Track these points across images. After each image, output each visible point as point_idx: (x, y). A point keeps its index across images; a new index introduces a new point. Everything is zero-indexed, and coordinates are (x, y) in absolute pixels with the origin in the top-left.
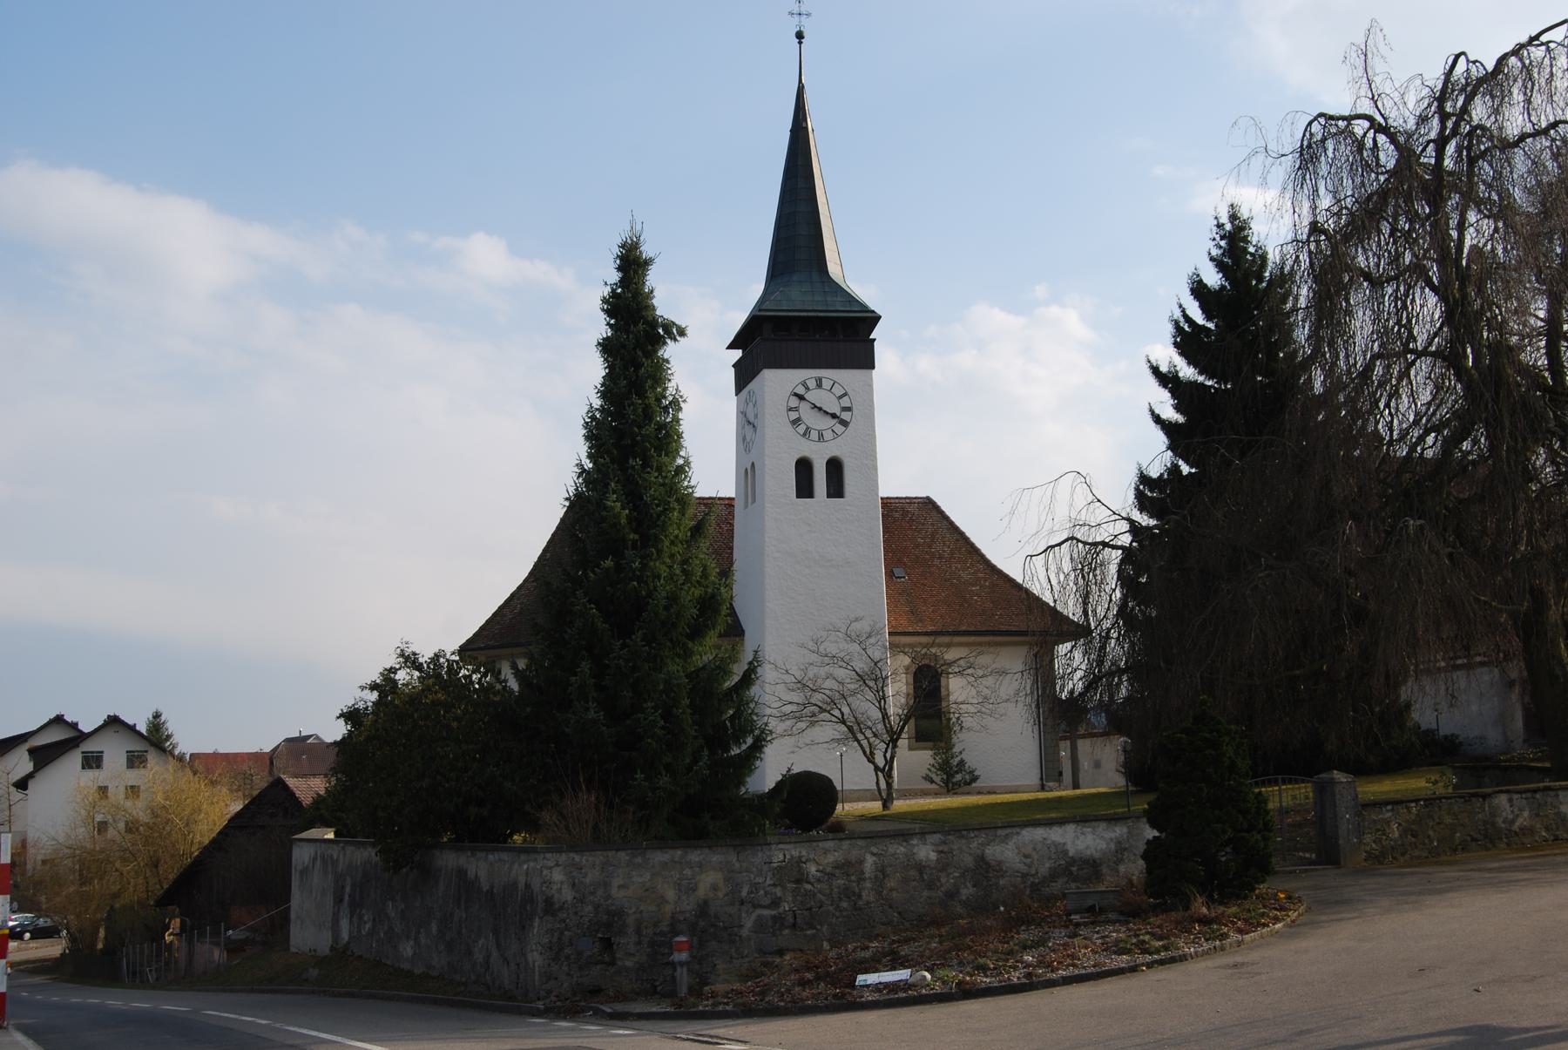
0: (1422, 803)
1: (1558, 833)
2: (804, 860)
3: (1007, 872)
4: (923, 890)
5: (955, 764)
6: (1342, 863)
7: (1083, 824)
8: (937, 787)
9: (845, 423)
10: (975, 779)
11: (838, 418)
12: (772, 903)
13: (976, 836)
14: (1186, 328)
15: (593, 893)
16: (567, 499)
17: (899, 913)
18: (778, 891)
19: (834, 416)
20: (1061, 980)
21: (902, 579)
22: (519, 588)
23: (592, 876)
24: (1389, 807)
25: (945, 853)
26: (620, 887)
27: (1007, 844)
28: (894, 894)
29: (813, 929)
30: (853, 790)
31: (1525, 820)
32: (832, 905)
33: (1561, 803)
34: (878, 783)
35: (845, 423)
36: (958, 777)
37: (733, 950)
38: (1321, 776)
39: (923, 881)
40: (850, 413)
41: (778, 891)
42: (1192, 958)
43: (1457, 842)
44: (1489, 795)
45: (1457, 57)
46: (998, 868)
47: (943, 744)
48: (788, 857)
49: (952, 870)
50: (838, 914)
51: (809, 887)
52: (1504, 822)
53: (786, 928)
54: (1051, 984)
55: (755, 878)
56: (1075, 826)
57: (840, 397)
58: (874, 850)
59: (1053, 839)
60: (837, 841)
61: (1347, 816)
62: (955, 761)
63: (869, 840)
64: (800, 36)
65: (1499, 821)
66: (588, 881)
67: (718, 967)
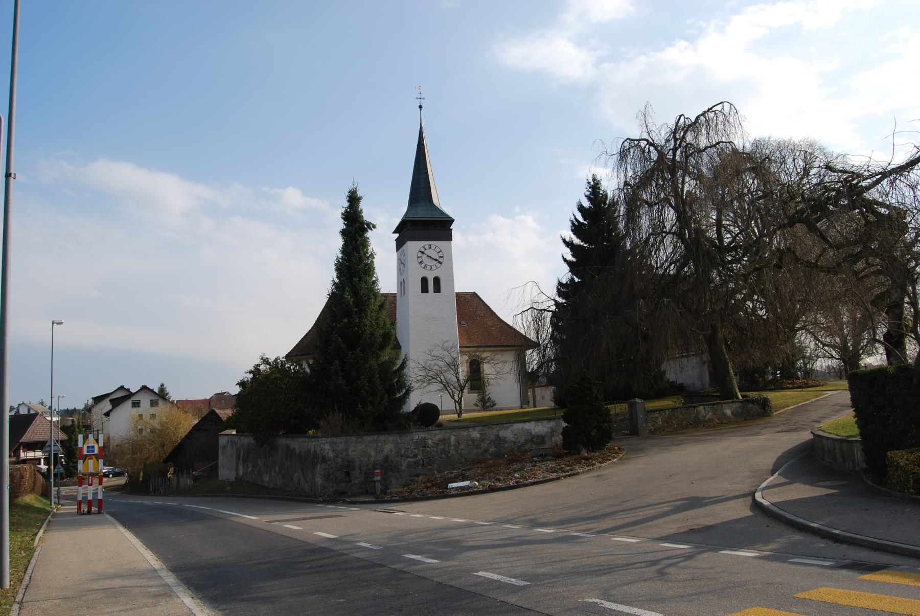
9: (440, 263)
10: (495, 405)
14: (576, 223)
15: (342, 454)
16: (328, 295)
17: (465, 459)
19: (436, 260)
23: (341, 446)
24: (658, 412)
26: (352, 451)
28: (463, 451)
34: (456, 407)
35: (440, 263)
36: (488, 404)
40: (442, 259)
41: (416, 451)
43: (684, 425)
45: (680, 116)
48: (420, 437)
51: (428, 449)
53: (420, 466)
54: (526, 485)
58: (454, 434)
64: (420, 107)
65: (700, 416)
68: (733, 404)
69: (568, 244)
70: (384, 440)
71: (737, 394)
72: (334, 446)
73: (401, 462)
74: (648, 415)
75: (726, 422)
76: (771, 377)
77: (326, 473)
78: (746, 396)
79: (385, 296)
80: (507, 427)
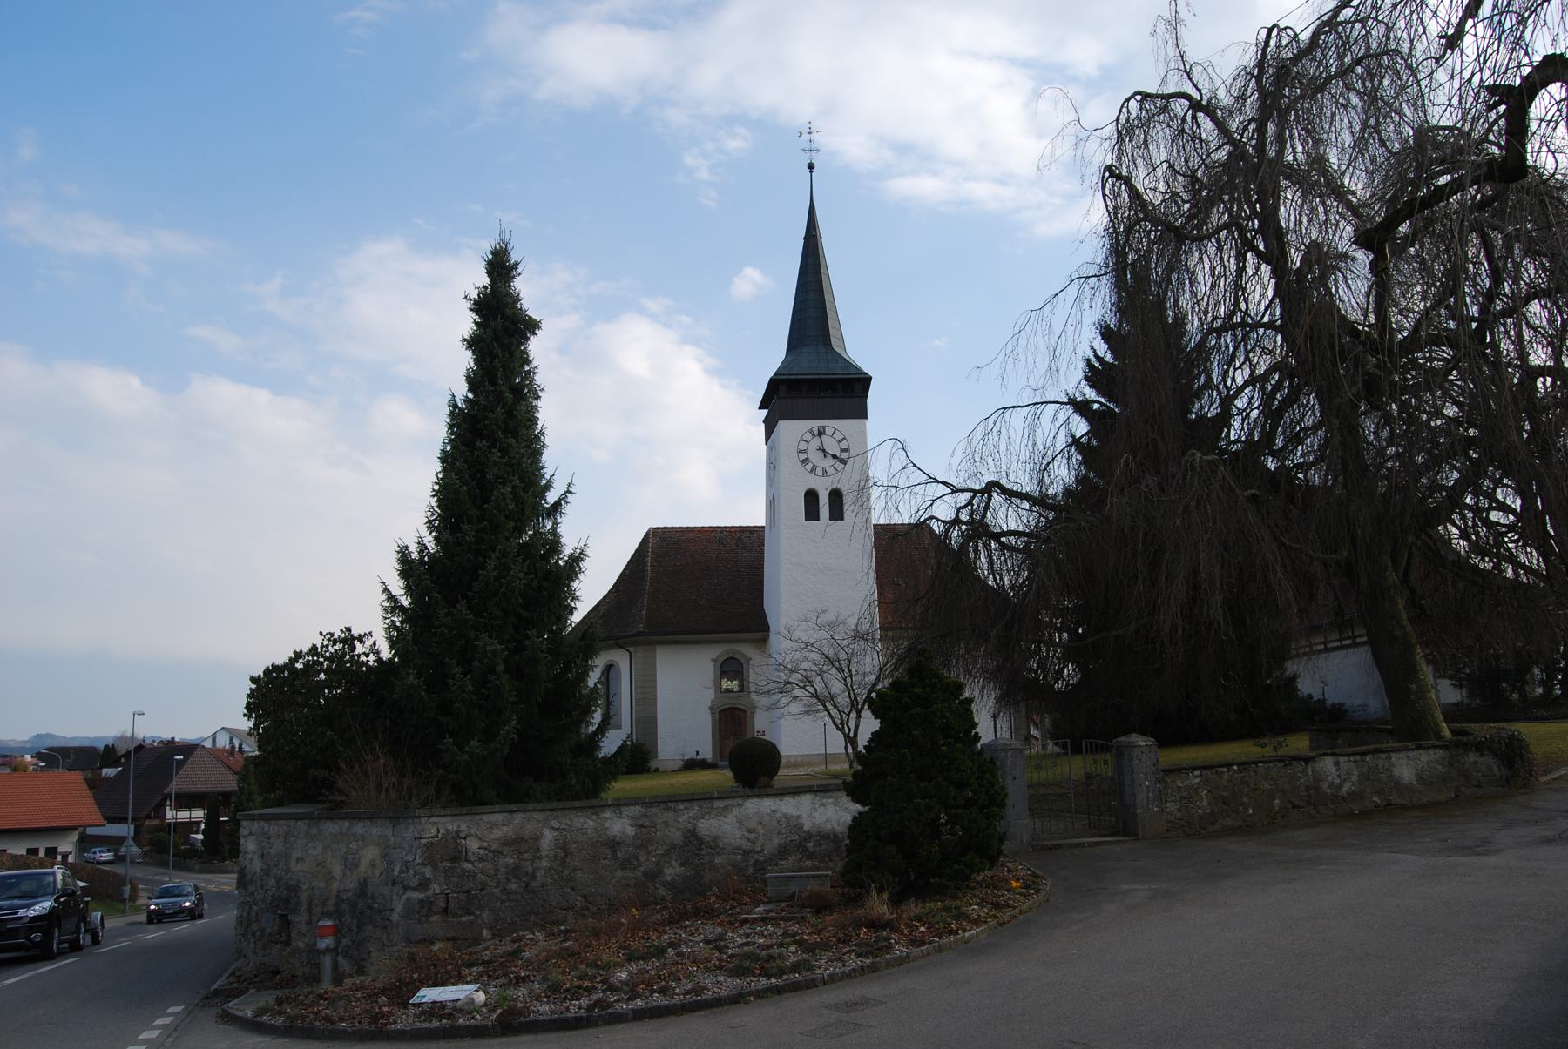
0: (1235, 767)
1: (1390, 797)
2: (462, 835)
3: (724, 849)
4: (617, 869)
6: (1140, 835)
7: (822, 794)
9: (844, 462)
12: (419, 885)
13: (686, 808)
14: (1097, 365)
15: (276, 865)
16: (436, 483)
17: (584, 896)
18: (428, 871)
20: (630, 1013)
23: (277, 847)
24: (1197, 773)
25: (645, 827)
26: (298, 860)
27: (726, 817)
28: (579, 874)
29: (470, 914)
31: (1354, 785)
32: (497, 887)
33: (1393, 766)
34: (846, 748)
35: (844, 462)
37: (385, 936)
38: (1119, 739)
39: (617, 859)
41: (428, 871)
42: (825, 984)
44: (1312, 759)
45: (1270, 30)
46: (713, 844)
48: (442, 832)
49: (654, 848)
50: (503, 897)
51: (468, 866)
52: (1330, 787)
53: (436, 914)
54: (619, 1019)
55: (406, 856)
56: (813, 796)
57: (840, 441)
58: (555, 824)
59: (784, 811)
60: (505, 814)
61: (1147, 783)
63: (548, 813)
64: (811, 167)
65: (1325, 786)
66: (273, 851)
67: (372, 954)
68: (1422, 752)
69: (1081, 407)
70: (363, 835)
71: (1437, 725)
72: (264, 844)
73: (392, 900)
74: (1166, 778)
75: (1400, 801)
76: (1540, 690)
77: (245, 915)
78: (1464, 733)
80: (725, 808)
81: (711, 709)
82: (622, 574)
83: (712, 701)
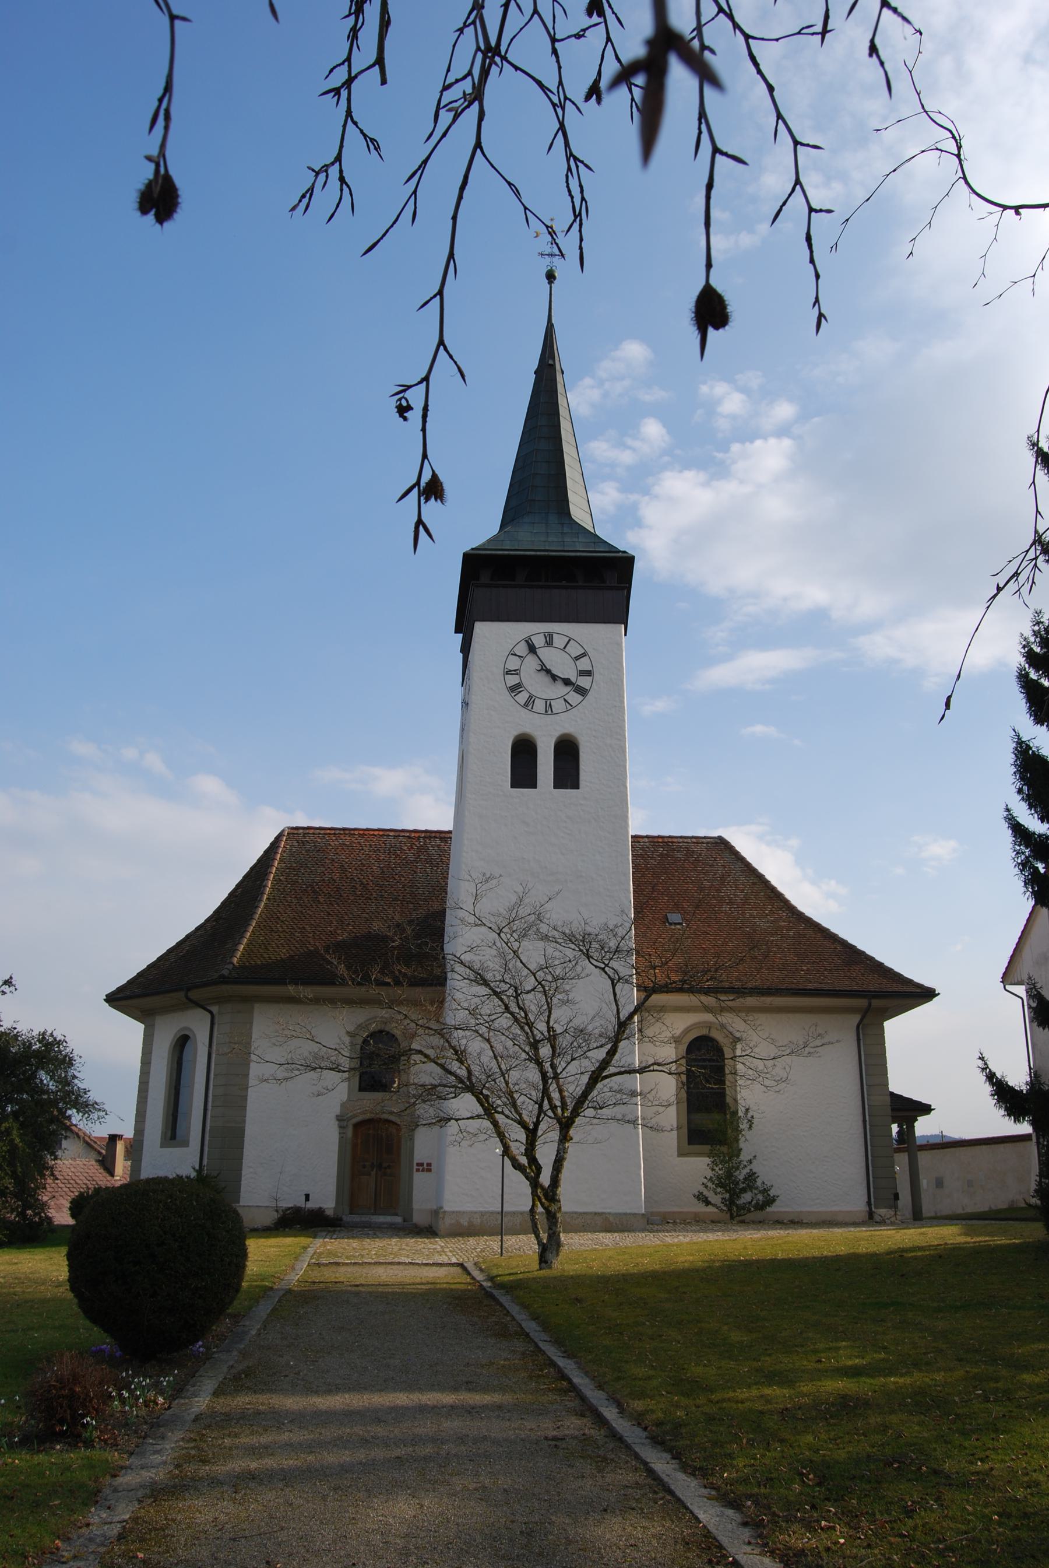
5: (741, 1177)
8: (716, 1210)
9: (582, 691)
10: (770, 1201)
11: (574, 684)
19: (567, 682)
21: (678, 926)
22: (198, 929)
30: (576, 1213)
35: (582, 691)
36: (747, 1197)
40: (589, 679)
47: (724, 1149)
57: (577, 658)
62: (741, 1175)
64: (551, 277)
79: (441, 838)
81: (339, 1118)
82: (231, 894)
83: (343, 1105)
